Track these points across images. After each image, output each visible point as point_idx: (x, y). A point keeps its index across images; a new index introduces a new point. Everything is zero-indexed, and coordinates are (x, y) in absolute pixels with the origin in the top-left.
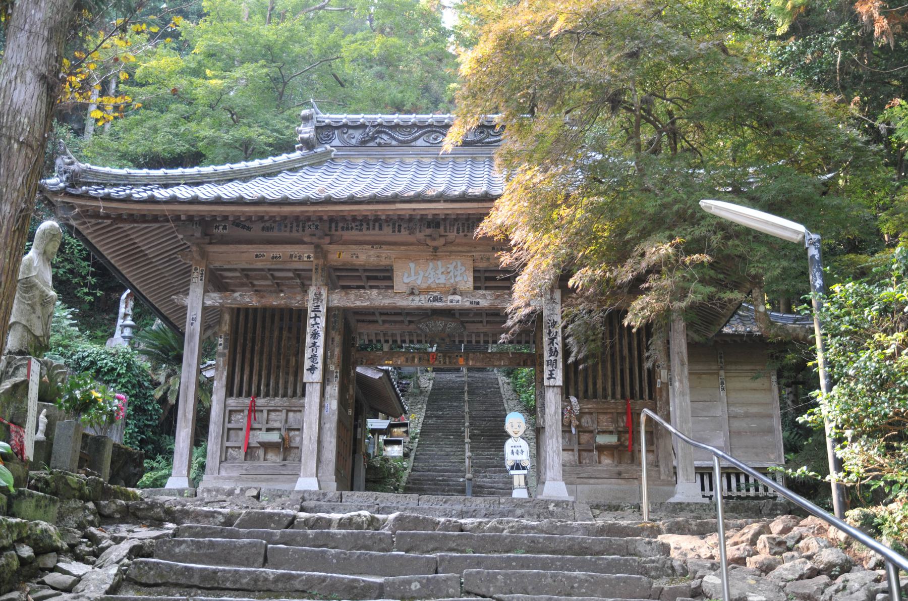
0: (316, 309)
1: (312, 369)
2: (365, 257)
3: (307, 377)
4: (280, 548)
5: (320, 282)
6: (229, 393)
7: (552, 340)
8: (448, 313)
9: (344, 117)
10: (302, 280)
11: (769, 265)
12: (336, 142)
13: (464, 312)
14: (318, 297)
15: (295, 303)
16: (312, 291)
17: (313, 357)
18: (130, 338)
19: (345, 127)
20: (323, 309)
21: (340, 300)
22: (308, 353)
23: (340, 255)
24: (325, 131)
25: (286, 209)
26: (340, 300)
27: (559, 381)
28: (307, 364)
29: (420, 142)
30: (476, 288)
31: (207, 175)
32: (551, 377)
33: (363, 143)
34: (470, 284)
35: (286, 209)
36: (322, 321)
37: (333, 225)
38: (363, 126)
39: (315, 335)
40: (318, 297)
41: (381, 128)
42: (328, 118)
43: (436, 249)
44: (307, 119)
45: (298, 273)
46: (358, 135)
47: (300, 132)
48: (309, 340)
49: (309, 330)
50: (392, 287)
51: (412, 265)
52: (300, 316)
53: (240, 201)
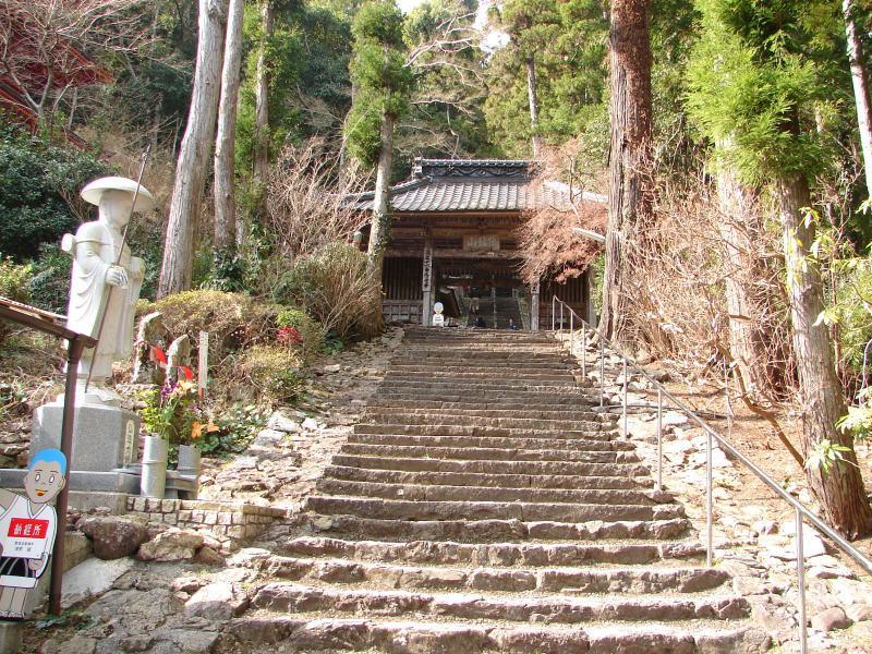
1: (426, 285)
2: (450, 233)
8: (489, 260)
10: (419, 244)
13: (494, 260)
14: (428, 252)
15: (418, 256)
16: (426, 249)
17: (427, 280)
18: (21, 399)
19: (436, 167)
21: (438, 254)
22: (424, 278)
23: (437, 232)
26: (438, 254)
27: (538, 292)
28: (424, 283)
30: (501, 248)
33: (446, 175)
34: (498, 247)
37: (557, 164)
38: (446, 166)
39: (427, 270)
40: (428, 252)
43: (482, 230)
44: (418, 163)
45: (417, 241)
47: (842, 452)
49: (424, 268)
50: (461, 248)
51: (472, 239)
52: (419, 263)
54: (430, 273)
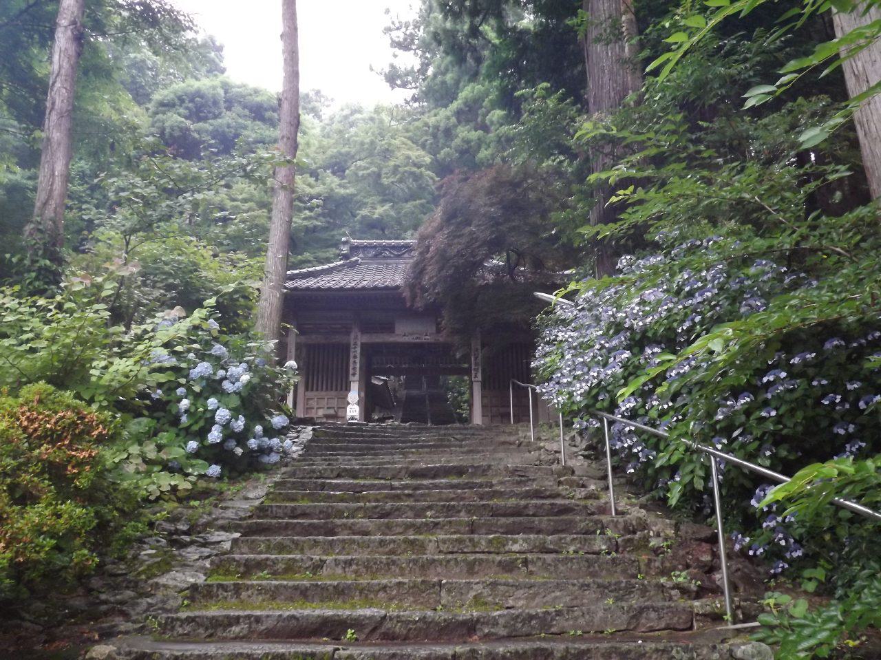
0: (355, 344)
1: (354, 374)
3: (351, 378)
4: (827, 76)
5: (356, 330)
6: (307, 389)
7: (476, 358)
9: (365, 242)
11: (799, 635)
12: (361, 255)
16: (352, 336)
17: (354, 369)
20: (359, 343)
24: (354, 249)
25: (353, 292)
28: (351, 371)
29: (406, 255)
31: (296, 275)
32: (476, 377)
33: (376, 256)
35: (353, 292)
36: (358, 350)
38: (375, 247)
39: (355, 357)
40: (356, 338)
41: (385, 248)
42: (356, 242)
44: (346, 243)
46: (373, 252)
48: (352, 360)
49: (352, 355)
52: (345, 349)
53: (308, 289)
54: (358, 360)
